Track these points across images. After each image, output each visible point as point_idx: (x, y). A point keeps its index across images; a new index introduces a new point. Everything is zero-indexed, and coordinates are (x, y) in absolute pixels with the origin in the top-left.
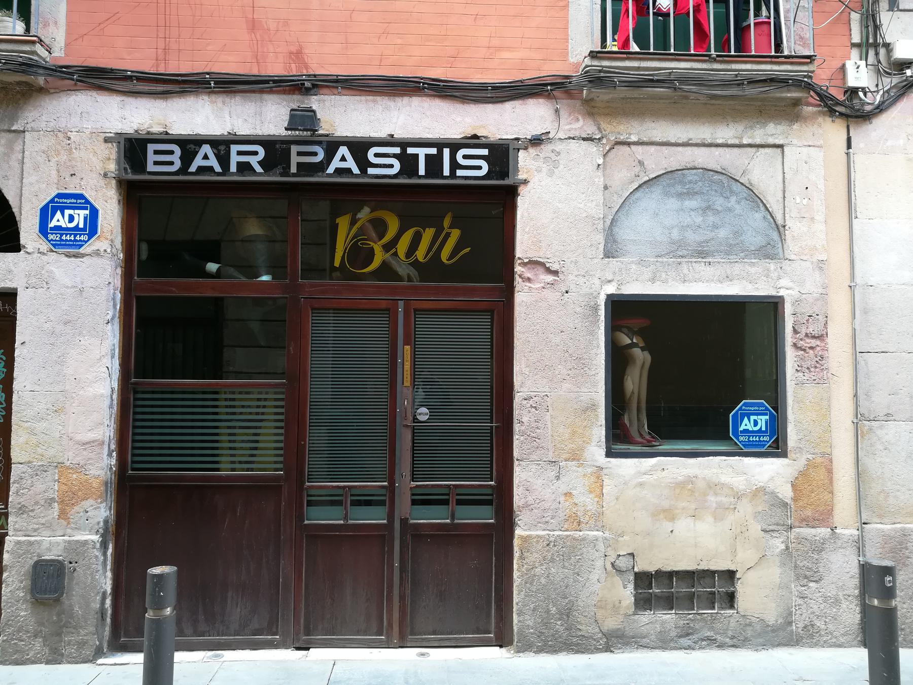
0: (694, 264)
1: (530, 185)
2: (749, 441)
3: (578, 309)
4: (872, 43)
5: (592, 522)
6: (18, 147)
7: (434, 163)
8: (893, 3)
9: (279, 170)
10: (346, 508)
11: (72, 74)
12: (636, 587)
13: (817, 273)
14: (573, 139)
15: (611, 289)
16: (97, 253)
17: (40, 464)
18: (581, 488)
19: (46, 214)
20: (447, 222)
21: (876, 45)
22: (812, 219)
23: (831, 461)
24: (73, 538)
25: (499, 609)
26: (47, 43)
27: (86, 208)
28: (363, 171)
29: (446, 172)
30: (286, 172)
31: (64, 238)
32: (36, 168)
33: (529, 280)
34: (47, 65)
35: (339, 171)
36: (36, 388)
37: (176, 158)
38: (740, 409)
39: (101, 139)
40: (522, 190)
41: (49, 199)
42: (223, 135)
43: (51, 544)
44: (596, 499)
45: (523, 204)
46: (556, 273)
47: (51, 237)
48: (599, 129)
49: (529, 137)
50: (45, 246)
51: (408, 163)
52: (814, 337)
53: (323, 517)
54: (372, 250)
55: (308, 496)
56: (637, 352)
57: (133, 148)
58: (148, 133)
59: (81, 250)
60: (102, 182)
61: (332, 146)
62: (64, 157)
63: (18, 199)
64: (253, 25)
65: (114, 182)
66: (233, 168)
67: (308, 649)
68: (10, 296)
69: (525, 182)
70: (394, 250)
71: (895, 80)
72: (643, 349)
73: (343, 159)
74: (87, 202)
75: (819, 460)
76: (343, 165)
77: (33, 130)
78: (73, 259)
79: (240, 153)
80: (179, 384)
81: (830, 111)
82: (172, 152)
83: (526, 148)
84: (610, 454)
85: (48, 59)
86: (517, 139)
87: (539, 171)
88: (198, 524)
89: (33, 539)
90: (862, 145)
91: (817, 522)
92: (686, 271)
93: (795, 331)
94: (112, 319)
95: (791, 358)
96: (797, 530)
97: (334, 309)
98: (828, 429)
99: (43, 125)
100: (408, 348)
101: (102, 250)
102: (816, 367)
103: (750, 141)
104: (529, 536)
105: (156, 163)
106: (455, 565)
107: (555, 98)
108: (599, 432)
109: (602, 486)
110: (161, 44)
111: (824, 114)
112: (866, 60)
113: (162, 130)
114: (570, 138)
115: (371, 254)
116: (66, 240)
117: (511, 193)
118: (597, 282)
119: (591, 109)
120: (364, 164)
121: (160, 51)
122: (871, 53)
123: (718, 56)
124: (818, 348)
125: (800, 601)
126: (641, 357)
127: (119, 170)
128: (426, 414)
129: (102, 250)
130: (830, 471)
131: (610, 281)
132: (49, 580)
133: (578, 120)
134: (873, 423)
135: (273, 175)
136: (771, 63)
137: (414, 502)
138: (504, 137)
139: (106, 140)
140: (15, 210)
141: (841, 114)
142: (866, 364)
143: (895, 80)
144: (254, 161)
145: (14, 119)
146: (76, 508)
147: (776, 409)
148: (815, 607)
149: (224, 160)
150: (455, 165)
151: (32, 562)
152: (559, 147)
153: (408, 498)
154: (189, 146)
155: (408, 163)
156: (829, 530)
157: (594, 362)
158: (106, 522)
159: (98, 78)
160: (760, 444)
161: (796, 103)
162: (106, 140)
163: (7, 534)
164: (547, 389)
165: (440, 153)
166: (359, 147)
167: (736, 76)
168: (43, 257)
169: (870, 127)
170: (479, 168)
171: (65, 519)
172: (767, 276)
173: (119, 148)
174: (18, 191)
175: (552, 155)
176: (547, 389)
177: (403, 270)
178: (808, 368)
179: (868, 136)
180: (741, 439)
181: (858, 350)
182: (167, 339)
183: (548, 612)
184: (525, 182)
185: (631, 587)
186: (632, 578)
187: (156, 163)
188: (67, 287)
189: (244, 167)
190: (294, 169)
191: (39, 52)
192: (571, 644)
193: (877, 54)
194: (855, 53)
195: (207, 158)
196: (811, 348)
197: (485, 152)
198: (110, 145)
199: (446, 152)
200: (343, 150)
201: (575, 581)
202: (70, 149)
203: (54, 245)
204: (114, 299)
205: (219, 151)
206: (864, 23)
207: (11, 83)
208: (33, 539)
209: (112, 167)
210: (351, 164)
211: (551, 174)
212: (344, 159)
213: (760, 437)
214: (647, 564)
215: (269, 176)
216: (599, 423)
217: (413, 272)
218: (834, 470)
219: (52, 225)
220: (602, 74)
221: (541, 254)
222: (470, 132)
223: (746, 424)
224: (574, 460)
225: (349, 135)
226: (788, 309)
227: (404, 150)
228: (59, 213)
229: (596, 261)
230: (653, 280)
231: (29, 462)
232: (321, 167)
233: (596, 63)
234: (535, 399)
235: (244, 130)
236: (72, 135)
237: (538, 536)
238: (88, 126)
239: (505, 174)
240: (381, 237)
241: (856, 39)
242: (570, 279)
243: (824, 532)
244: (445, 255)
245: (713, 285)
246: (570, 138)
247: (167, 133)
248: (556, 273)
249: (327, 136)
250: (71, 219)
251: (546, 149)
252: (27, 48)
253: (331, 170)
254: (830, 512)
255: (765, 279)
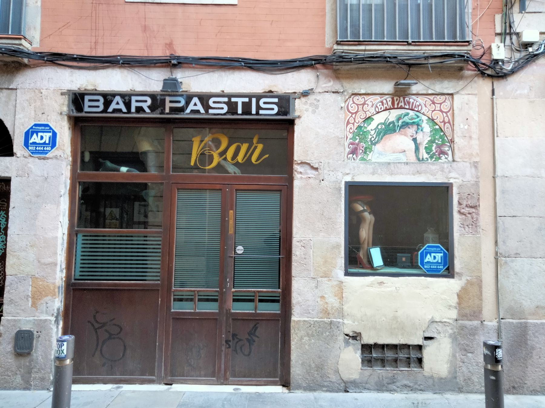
0: (398, 164)
1: (302, 119)
2: (431, 268)
3: (329, 190)
4: (508, 32)
5: (336, 314)
6: (13, 98)
7: (247, 107)
8: (523, 8)
9: (159, 110)
10: (195, 303)
11: (44, 57)
12: (363, 353)
13: (473, 170)
14: (327, 92)
15: (349, 179)
16: (56, 157)
17: (22, 276)
18: (335, 296)
19: (28, 135)
20: (255, 141)
21: (510, 34)
22: (471, 137)
23: (481, 281)
24: (39, 318)
25: (283, 364)
26: (30, 39)
27: (50, 132)
28: (207, 112)
29: (254, 111)
30: (162, 113)
31: (37, 148)
32: (23, 109)
33: (301, 173)
34: (29, 52)
35: (193, 111)
36: (20, 233)
37: (101, 104)
38: (425, 249)
39: (60, 94)
40: (297, 122)
41: (30, 127)
42: (127, 91)
43: (26, 323)
44: (339, 300)
45: (298, 129)
46: (316, 169)
47: (30, 148)
48: (342, 86)
49: (301, 91)
50: (27, 153)
51: (232, 107)
52: (471, 207)
53: (176, 308)
54: (212, 155)
55: (174, 295)
56: (367, 215)
57: (77, 99)
58: (86, 90)
59: (47, 156)
60: (59, 117)
61: (189, 98)
62: (38, 103)
63: (13, 126)
64: (145, 28)
65: (66, 117)
66: (133, 110)
67: (171, 384)
68: (7, 181)
69: (299, 117)
70: (225, 156)
71: (523, 54)
72: (370, 213)
73: (195, 105)
74: (51, 128)
75: (475, 280)
76: (195, 108)
77: (22, 88)
78: (42, 160)
79: (137, 101)
80: (101, 231)
81: (482, 74)
82: (98, 101)
83: (299, 98)
84: (347, 274)
85: (30, 49)
86: (295, 93)
87: (307, 110)
88: (115, 312)
89: (16, 318)
90: (501, 93)
91: (473, 317)
92: (393, 168)
93: (460, 204)
94: (64, 194)
95: (457, 218)
96: (461, 322)
97: (210, 190)
98: (479, 262)
99: (27, 86)
100: (231, 211)
101: (58, 155)
102: (472, 225)
103: (433, 92)
104: (299, 321)
105: (90, 107)
106: (257, 336)
107: (317, 69)
108: (341, 261)
109: (342, 293)
110: (93, 40)
111: (476, 75)
112: (504, 43)
113: (93, 88)
114: (325, 92)
115: (211, 158)
116: (39, 150)
117: (292, 122)
118: (340, 174)
119: (337, 76)
120: (207, 107)
121: (93, 44)
122: (508, 38)
123: (413, 42)
124: (474, 214)
125: (461, 364)
126: (369, 217)
127: (69, 110)
128: (242, 250)
129: (58, 155)
130: (480, 287)
131: (347, 174)
132: (24, 343)
133: (330, 81)
134: (507, 259)
135: (156, 114)
136: (445, 45)
137: (234, 300)
138: (287, 92)
139: (62, 94)
140: (11, 133)
141: (489, 76)
142: (503, 223)
143: (523, 54)
144: (145, 106)
145: (11, 82)
146: (42, 301)
147: (448, 250)
148: (471, 368)
149: (128, 105)
150: (258, 108)
151: (15, 331)
152: (319, 97)
153: (231, 298)
154: (108, 97)
155: (232, 107)
156: (480, 322)
157: (338, 221)
158: (58, 310)
159: (55, 59)
160: (438, 270)
161: (461, 69)
162: (62, 94)
163: (2, 316)
164: (311, 236)
165: (250, 101)
166: (204, 98)
167: (424, 53)
168: (25, 159)
169: (507, 82)
170: (265, 103)
171: (35, 307)
172: (442, 171)
173: (69, 98)
174: (13, 122)
175: (316, 103)
176: (311, 236)
177: (232, 169)
178: (467, 226)
179: (504, 87)
180: (425, 267)
181: (498, 215)
182: (99, 204)
183: (310, 366)
184: (299, 117)
185: (359, 352)
186: (360, 347)
187: (90, 107)
188: (39, 176)
189: (139, 110)
190: (167, 110)
191: (23, 44)
192: (324, 386)
193: (511, 39)
194: (497, 39)
195: (118, 104)
196: (470, 213)
197: (276, 100)
198: (64, 96)
199: (254, 100)
200: (195, 100)
201: (326, 348)
202: (39, 101)
203: (32, 153)
204: (65, 183)
205: (125, 100)
206: (504, 21)
207: (9, 62)
208: (16, 318)
209: (65, 109)
210: (200, 107)
211: (314, 112)
212: (196, 105)
213: (437, 266)
214: (369, 339)
215: (153, 114)
216: (340, 256)
217: (237, 170)
218: (483, 286)
219: (31, 141)
220: (343, 54)
221: (308, 158)
222: (269, 90)
223: (429, 258)
224: (326, 277)
225: (199, 91)
226: (455, 190)
227: (230, 100)
228: (35, 134)
229: (340, 162)
230: (373, 173)
231: (16, 275)
232: (182, 110)
233: (340, 47)
234: (304, 242)
235: (139, 88)
236: (43, 91)
237: (304, 321)
238: (52, 86)
239: (286, 113)
240: (217, 149)
241: (498, 30)
242: (325, 172)
243: (476, 323)
244: (254, 159)
245: (409, 176)
246: (325, 92)
247: (96, 90)
248: (316, 169)
249: (186, 91)
250: (42, 138)
251: (311, 98)
252: (17, 42)
253: (188, 111)
254: (480, 312)
255: (441, 173)
